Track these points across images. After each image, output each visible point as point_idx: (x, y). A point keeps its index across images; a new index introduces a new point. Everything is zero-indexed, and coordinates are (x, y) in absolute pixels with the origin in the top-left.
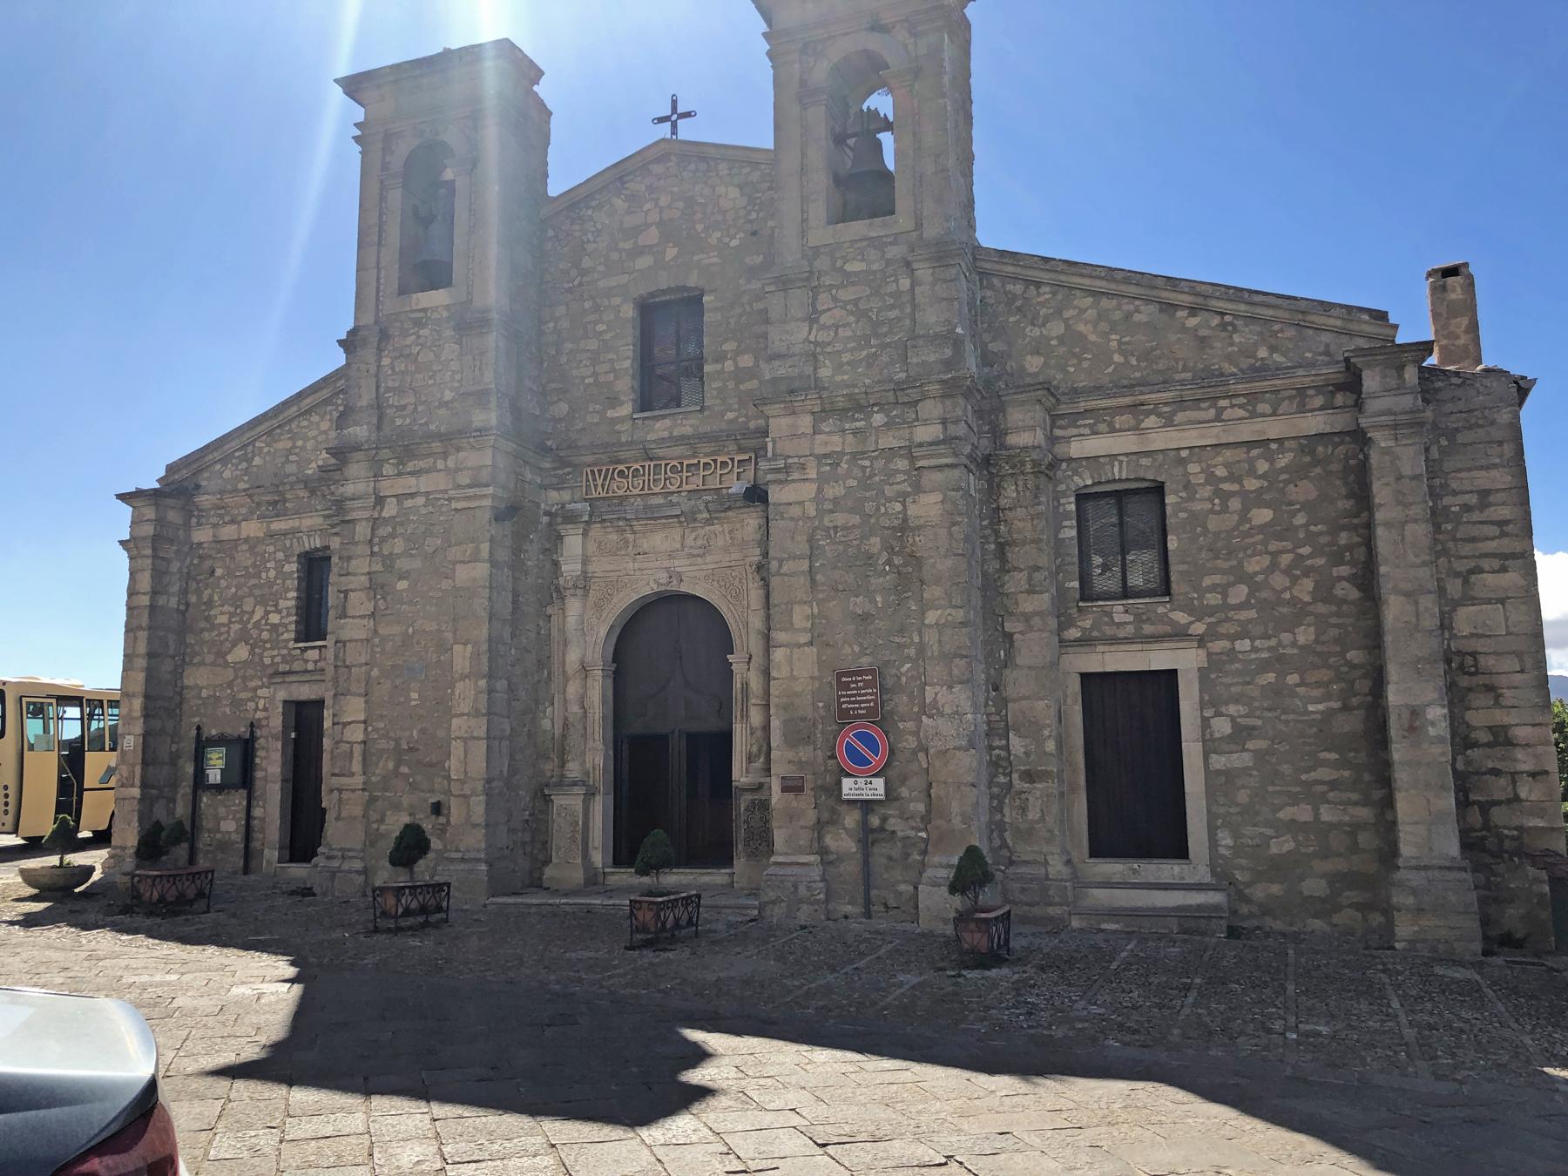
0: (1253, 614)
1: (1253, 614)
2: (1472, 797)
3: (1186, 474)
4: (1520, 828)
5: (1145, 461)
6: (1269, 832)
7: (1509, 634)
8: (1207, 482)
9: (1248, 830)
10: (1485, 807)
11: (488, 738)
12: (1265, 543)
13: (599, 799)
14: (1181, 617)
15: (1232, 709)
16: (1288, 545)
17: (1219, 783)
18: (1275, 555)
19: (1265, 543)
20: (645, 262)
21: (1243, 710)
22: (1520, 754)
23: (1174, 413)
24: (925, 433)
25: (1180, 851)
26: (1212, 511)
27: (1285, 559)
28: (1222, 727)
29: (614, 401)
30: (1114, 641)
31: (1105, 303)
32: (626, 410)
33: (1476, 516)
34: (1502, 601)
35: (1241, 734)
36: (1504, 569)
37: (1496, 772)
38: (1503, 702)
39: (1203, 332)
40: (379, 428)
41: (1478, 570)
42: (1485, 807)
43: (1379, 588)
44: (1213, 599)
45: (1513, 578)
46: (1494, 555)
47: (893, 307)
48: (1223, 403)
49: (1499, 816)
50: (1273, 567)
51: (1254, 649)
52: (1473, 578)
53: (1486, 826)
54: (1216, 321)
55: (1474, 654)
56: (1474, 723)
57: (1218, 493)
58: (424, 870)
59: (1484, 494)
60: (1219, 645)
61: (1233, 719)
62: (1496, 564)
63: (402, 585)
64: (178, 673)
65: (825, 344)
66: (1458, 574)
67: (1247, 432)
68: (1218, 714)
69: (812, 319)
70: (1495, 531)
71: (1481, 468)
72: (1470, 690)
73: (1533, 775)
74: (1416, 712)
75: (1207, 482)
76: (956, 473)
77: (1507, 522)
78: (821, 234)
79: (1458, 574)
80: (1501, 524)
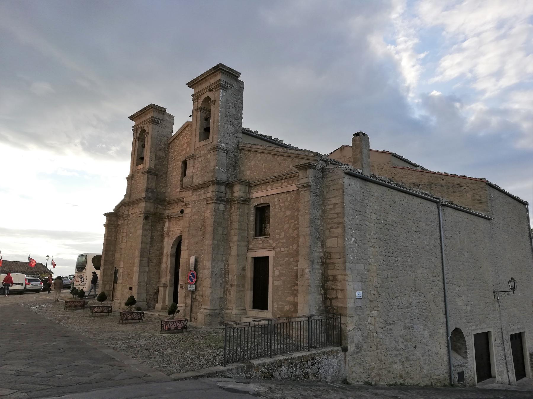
1: (285, 241)
2: (328, 296)
5: (267, 198)
6: (285, 304)
8: (278, 204)
9: (280, 303)
10: (331, 299)
14: (271, 241)
16: (293, 221)
20: (184, 152)
21: (281, 268)
22: (339, 284)
23: (273, 185)
24: (209, 195)
25: (266, 308)
26: (279, 212)
27: (292, 225)
28: (277, 273)
29: (177, 188)
30: (258, 249)
31: (263, 155)
32: (178, 190)
34: (337, 237)
35: (281, 275)
36: (338, 227)
37: (333, 289)
38: (336, 267)
39: (280, 162)
41: (332, 228)
42: (331, 299)
44: (277, 236)
45: (109, 238)
48: (283, 181)
49: (334, 303)
50: (290, 227)
52: (332, 230)
53: (331, 305)
58: (107, 303)
59: (335, 205)
61: (279, 271)
64: (113, 255)
67: (286, 190)
68: (277, 269)
70: (336, 216)
71: (334, 197)
72: (329, 263)
73: (341, 290)
74: (303, 270)
75: (278, 204)
76: (213, 205)
77: (340, 213)
79: (328, 229)
80: (338, 214)
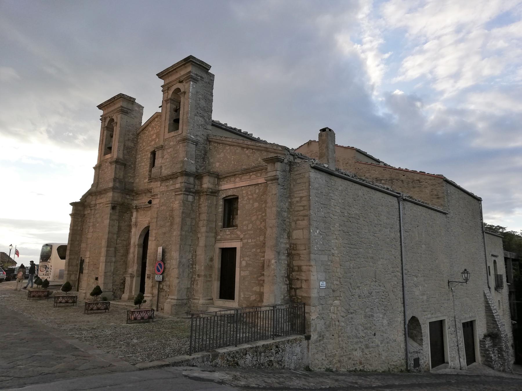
0: (252, 232)
2: (293, 286)
3: (243, 194)
4: (302, 296)
5: (235, 190)
7: (303, 238)
10: (296, 289)
11: (106, 262)
12: (256, 212)
13: (135, 279)
15: (246, 259)
17: (243, 278)
18: (258, 216)
19: (256, 212)
20: (153, 143)
23: (241, 177)
27: (260, 216)
31: (232, 147)
32: (147, 180)
33: (299, 205)
34: (303, 229)
36: (304, 220)
38: (301, 258)
39: (249, 154)
40: (97, 187)
42: (296, 289)
43: (71, 221)
44: (245, 228)
46: (302, 216)
47: (176, 153)
51: (252, 242)
53: (296, 295)
54: (251, 151)
55: (296, 244)
56: (295, 265)
57: (248, 198)
60: (245, 241)
62: (302, 218)
63: (98, 225)
65: (163, 163)
66: (294, 221)
68: (244, 260)
69: (163, 157)
70: (302, 208)
71: (301, 190)
72: (295, 255)
73: (306, 281)
74: (270, 261)
78: (167, 135)
79: (294, 221)
80: (304, 206)
